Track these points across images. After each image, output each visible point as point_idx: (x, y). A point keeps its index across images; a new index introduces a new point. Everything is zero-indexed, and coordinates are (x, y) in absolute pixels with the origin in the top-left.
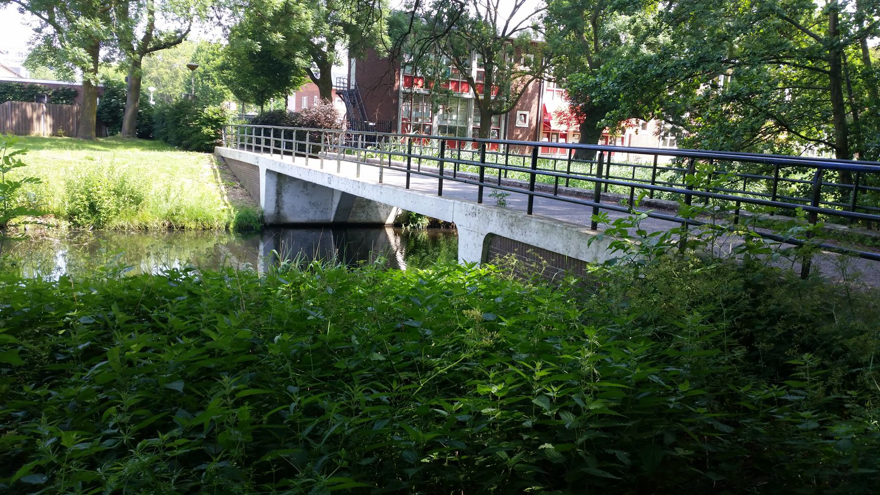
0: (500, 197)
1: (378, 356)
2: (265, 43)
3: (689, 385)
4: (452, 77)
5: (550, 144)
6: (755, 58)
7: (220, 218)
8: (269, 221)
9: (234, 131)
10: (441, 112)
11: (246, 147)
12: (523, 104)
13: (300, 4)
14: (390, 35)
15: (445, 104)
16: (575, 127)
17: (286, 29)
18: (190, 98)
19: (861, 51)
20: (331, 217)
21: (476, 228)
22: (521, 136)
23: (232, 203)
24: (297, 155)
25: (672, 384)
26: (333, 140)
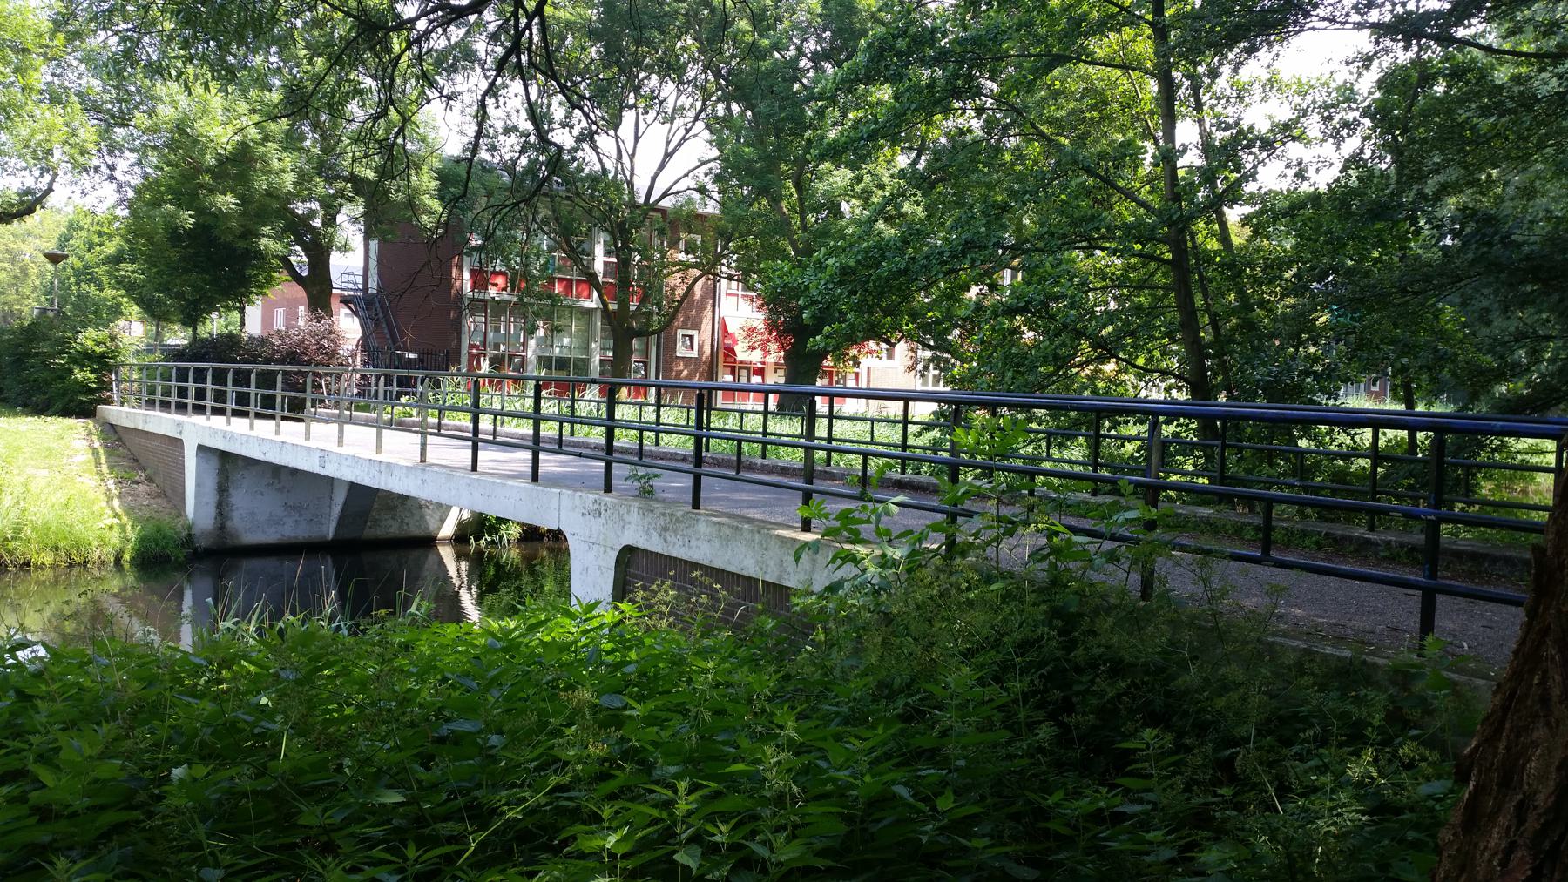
0: (643, 481)
1: (393, 798)
2: (201, 212)
3: (952, 798)
4: (559, 270)
5: (736, 385)
6: (1055, 241)
7: (103, 542)
8: (203, 543)
9: (135, 376)
10: (541, 333)
11: (158, 404)
12: (687, 318)
13: (270, 144)
14: (441, 198)
15: (548, 318)
16: (775, 355)
17: (240, 189)
18: (51, 314)
19: (1216, 227)
20: (329, 530)
21: (602, 537)
22: (685, 373)
23: (129, 511)
24: (258, 416)
25: (925, 800)
26: (334, 387)
